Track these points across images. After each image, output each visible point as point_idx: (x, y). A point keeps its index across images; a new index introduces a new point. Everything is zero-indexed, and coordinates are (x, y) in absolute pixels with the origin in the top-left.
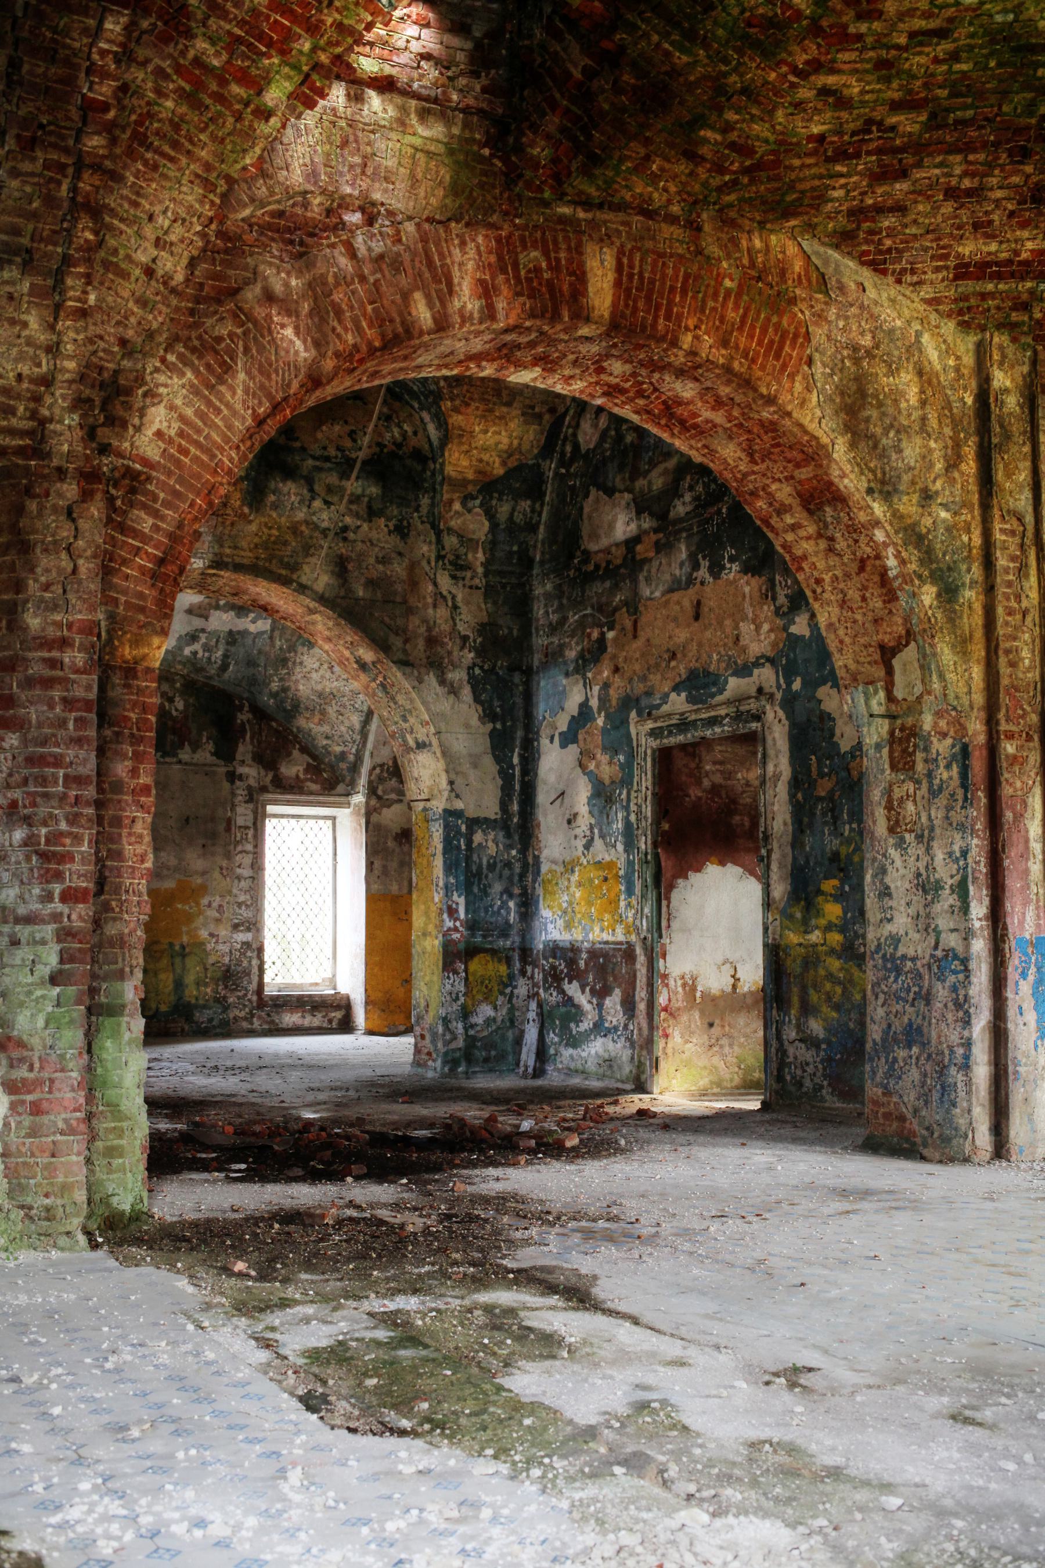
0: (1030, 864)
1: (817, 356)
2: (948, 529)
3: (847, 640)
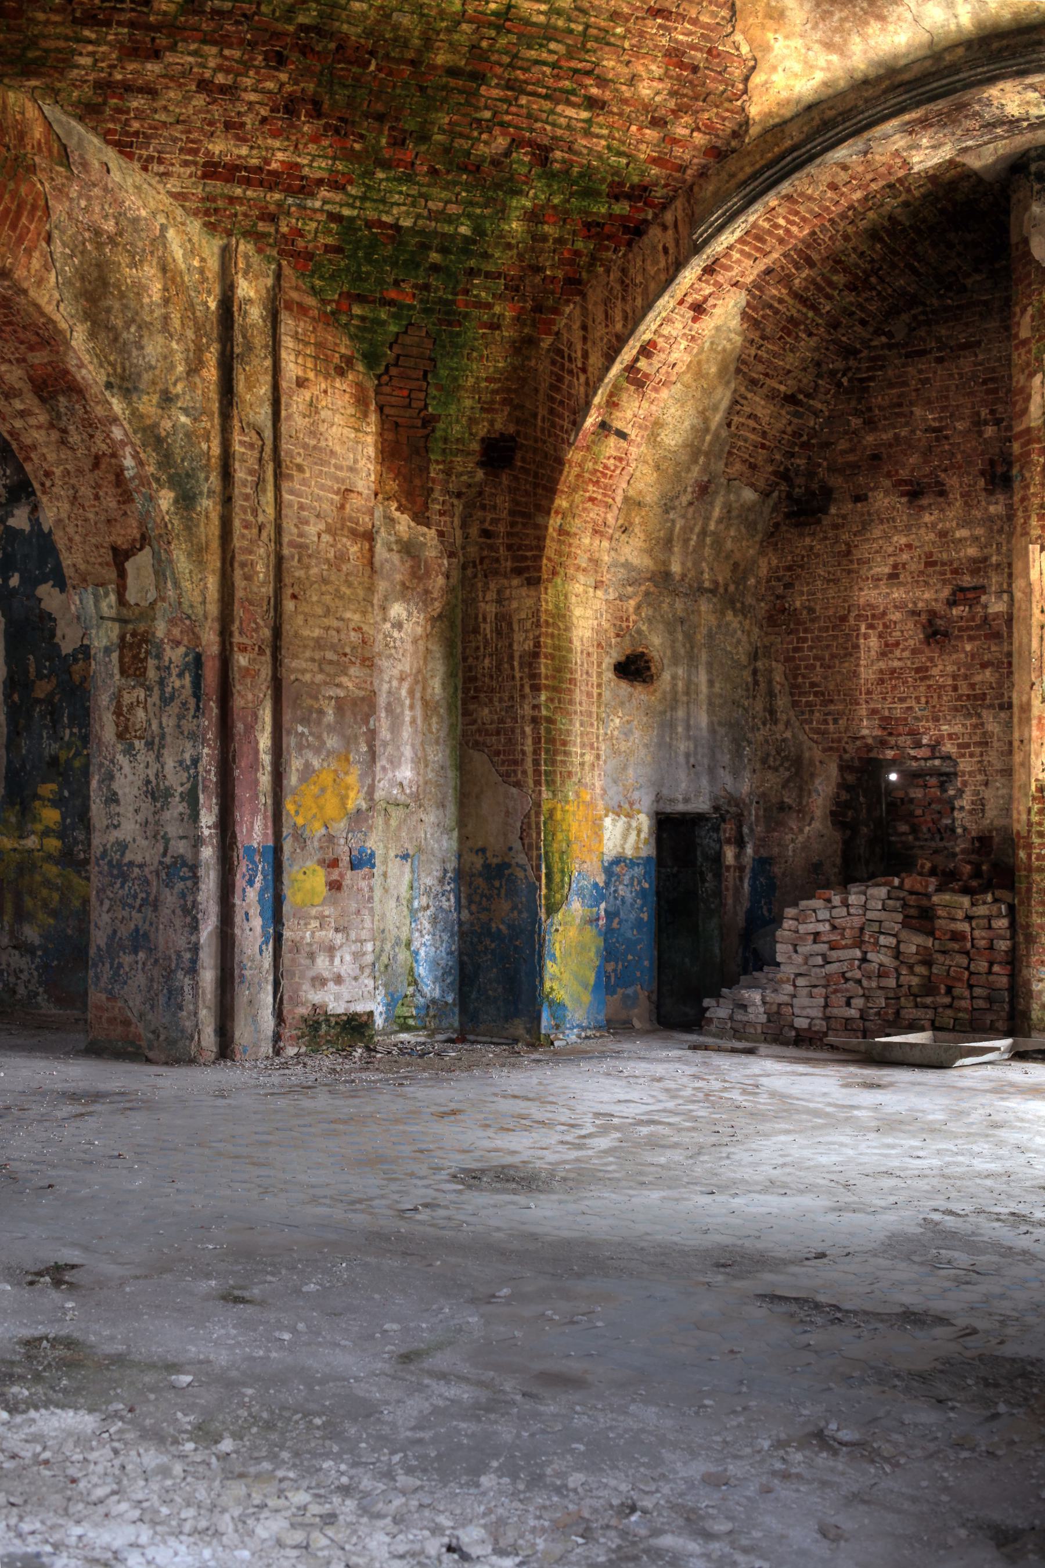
0: (259, 775)
1: (56, 234)
2: (188, 435)
3: (77, 538)
